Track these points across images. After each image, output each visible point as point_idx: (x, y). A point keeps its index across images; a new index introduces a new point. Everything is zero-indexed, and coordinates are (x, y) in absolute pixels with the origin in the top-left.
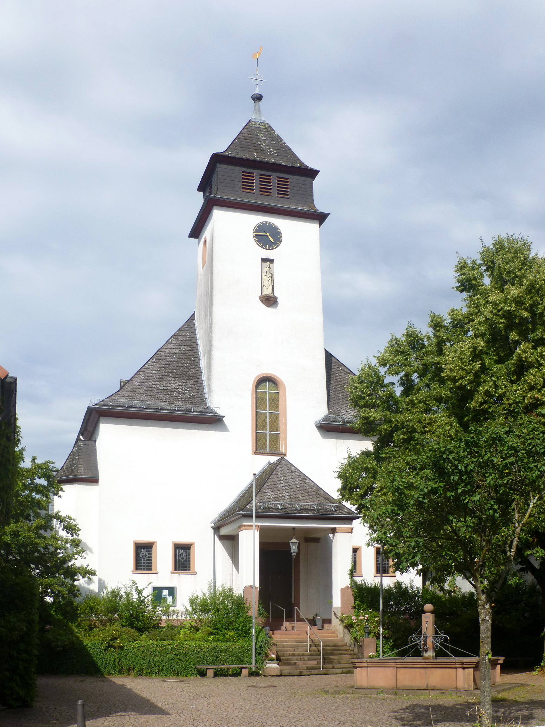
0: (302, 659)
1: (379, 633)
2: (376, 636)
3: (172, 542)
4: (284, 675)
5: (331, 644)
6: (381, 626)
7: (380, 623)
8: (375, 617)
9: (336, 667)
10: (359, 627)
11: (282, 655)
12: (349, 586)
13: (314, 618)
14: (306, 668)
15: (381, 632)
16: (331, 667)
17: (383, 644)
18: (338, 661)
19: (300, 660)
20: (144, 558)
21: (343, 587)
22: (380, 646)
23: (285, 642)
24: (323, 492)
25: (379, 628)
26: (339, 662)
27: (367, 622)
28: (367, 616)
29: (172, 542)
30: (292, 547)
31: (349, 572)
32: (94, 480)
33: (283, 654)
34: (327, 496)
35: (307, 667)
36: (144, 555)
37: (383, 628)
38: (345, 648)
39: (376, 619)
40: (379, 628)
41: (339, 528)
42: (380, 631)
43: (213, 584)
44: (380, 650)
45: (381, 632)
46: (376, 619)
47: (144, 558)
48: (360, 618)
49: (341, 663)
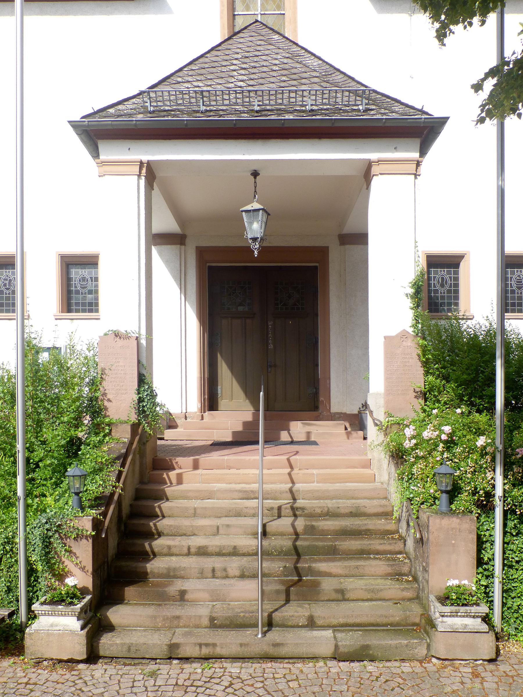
0: (218, 574)
1: (489, 495)
2: (479, 505)
3: (57, 252)
4: (107, 653)
5: (345, 505)
6: (499, 470)
7: (493, 460)
8: (479, 433)
9: (319, 622)
10: (421, 464)
11: (165, 551)
12: (411, 330)
13: (360, 412)
14: (206, 622)
15: (499, 492)
16: (303, 621)
17: (505, 533)
18: (337, 591)
19: (214, 577)
20: (8, 289)
21: (393, 332)
22: (492, 543)
23: (210, 495)
24: (342, 76)
25: (489, 475)
26: (341, 592)
27: (448, 449)
28: (447, 429)
29: (57, 252)
30: (251, 223)
31: (411, 291)
32: (385, 337)
33: (169, 547)
34: (354, 86)
35: (212, 619)
36: (7, 282)
37: (505, 477)
38: (381, 524)
39: (481, 441)
40: (489, 475)
41: (379, 161)
42: (494, 486)
43: (143, 342)
44: (492, 559)
45: (499, 492)
46: (481, 441)
47: (8, 289)
48: (427, 434)
49: (350, 595)
